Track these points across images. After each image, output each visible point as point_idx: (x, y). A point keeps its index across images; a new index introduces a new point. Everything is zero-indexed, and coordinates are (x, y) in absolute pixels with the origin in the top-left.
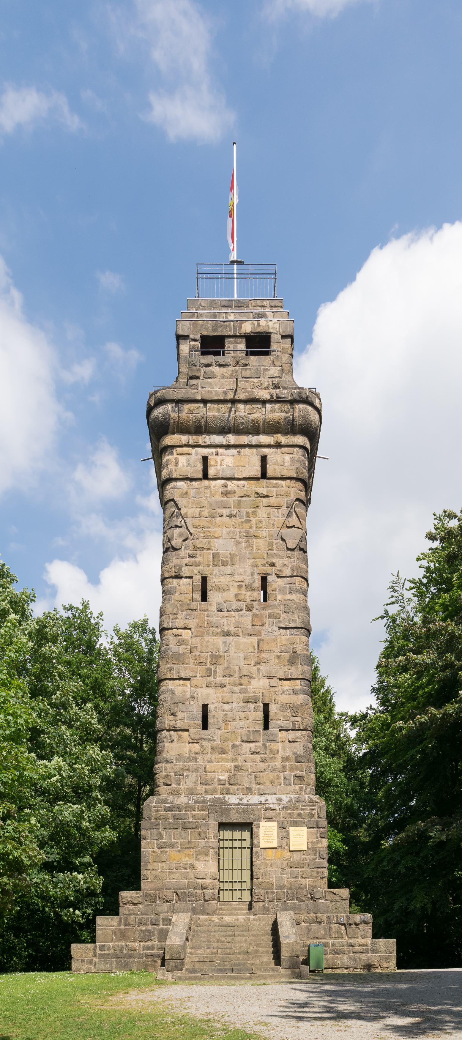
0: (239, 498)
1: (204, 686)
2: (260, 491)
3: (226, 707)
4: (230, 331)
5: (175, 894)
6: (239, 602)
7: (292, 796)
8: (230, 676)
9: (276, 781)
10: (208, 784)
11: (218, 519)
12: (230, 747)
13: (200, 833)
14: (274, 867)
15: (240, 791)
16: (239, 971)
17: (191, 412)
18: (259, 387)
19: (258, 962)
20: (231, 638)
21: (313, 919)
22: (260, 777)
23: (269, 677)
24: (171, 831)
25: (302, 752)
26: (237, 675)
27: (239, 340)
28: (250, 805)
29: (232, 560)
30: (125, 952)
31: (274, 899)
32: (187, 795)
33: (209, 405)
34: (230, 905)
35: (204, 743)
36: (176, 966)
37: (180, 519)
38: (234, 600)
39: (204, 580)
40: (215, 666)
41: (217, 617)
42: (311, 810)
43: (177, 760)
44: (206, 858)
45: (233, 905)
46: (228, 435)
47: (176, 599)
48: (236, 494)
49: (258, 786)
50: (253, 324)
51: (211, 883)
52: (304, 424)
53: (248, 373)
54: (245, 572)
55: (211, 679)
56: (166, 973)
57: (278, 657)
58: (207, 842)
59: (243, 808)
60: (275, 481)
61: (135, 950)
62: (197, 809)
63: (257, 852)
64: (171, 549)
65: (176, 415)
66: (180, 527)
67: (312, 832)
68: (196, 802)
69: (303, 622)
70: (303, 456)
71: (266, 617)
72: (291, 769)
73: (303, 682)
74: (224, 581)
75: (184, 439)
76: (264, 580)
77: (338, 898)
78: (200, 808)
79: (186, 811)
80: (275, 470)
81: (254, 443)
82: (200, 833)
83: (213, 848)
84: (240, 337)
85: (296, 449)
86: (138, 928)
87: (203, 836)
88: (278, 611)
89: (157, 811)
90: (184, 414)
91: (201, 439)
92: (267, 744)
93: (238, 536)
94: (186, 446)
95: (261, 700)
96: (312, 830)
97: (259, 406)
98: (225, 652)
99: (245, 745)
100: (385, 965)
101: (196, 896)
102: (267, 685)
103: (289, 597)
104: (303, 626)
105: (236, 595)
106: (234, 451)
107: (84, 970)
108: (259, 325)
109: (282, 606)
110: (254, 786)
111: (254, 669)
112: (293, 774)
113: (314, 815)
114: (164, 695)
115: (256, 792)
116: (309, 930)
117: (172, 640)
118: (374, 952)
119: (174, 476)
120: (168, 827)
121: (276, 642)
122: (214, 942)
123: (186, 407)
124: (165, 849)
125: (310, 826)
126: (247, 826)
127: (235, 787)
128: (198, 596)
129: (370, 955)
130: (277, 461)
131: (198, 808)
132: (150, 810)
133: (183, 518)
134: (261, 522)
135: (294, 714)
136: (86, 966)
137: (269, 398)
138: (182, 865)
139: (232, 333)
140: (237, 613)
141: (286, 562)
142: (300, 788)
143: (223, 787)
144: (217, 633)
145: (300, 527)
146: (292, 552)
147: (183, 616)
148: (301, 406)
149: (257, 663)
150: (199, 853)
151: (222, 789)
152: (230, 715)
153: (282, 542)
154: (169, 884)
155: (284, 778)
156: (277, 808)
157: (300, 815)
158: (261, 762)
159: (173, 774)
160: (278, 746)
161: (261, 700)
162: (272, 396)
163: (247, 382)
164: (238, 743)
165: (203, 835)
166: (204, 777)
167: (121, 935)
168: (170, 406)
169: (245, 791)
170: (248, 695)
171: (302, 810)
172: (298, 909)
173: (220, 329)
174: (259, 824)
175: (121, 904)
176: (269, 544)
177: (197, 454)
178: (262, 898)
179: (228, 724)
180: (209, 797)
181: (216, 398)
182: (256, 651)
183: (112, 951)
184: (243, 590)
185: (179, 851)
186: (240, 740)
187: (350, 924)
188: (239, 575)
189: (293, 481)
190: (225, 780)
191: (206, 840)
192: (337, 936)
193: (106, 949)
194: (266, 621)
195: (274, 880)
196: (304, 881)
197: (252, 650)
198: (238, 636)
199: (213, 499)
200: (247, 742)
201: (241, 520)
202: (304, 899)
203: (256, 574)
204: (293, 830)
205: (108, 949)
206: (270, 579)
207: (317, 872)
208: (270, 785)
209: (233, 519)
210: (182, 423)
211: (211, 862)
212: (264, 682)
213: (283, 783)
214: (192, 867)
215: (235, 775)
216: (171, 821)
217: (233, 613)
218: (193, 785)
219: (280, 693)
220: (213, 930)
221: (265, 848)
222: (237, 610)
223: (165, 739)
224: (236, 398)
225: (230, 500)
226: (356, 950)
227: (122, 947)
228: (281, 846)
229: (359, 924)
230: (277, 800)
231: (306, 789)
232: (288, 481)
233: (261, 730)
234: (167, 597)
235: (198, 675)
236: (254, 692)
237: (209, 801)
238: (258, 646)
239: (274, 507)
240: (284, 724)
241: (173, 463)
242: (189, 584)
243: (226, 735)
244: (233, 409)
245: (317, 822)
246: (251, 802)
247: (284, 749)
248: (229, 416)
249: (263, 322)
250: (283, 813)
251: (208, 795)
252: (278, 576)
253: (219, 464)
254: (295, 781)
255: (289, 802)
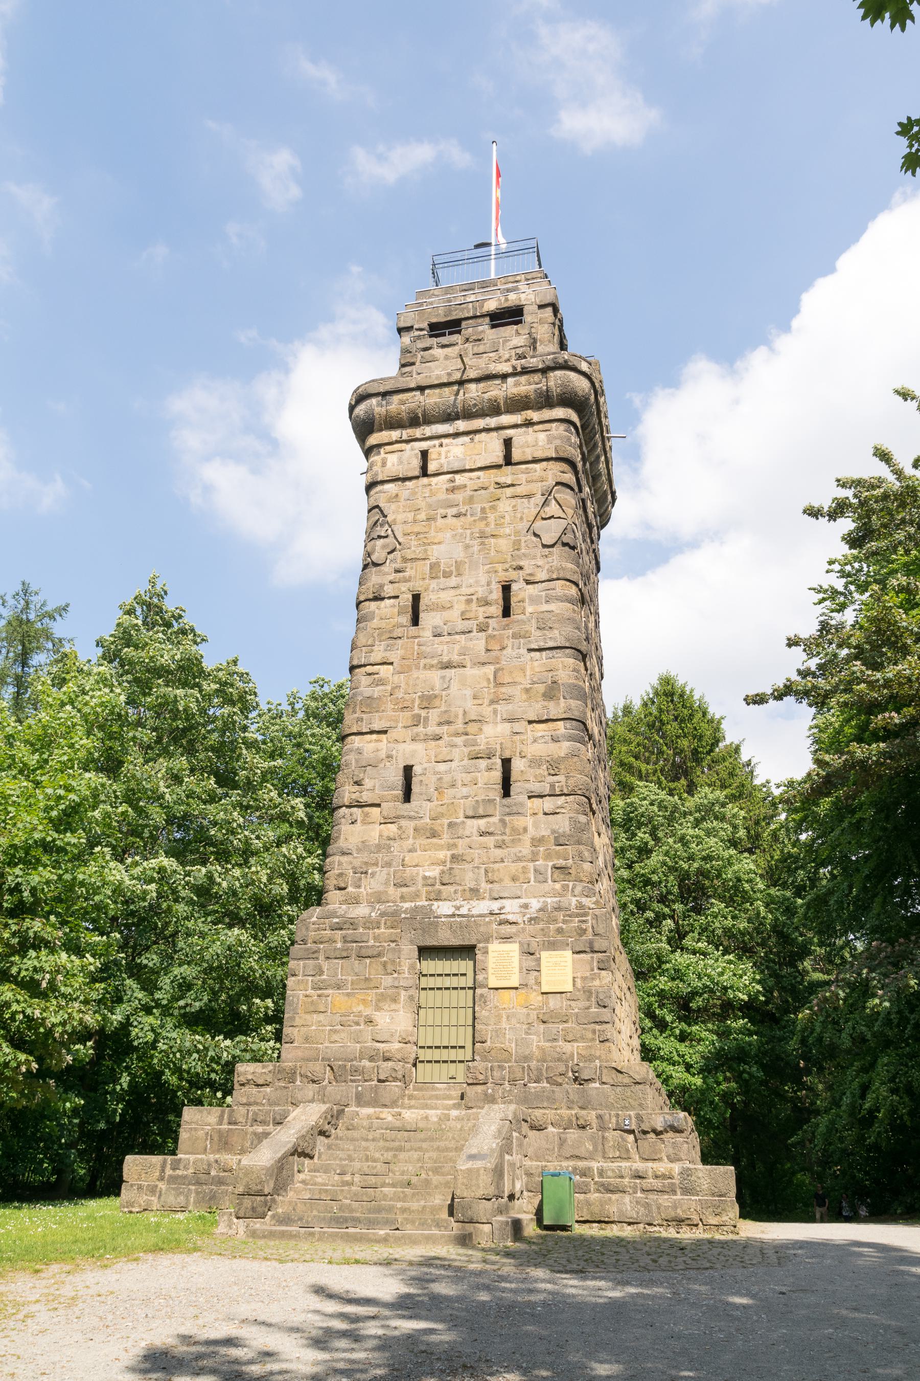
0: (472, 493)
1: (408, 740)
2: (502, 480)
3: (442, 767)
4: (468, 312)
5: (328, 1068)
6: (467, 622)
7: (549, 900)
8: (449, 723)
9: (522, 876)
10: (406, 885)
11: (440, 521)
12: (446, 827)
13: (384, 965)
14: (514, 1021)
15: (459, 894)
16: (371, 1223)
17: (403, 403)
18: (498, 360)
19: (415, 1205)
20: (453, 670)
21: (570, 1121)
22: (493, 871)
23: (511, 720)
24: (337, 961)
25: (567, 829)
26: (460, 720)
27: (480, 320)
28: (473, 916)
29: (457, 569)
30: (213, 1173)
31: (504, 1079)
32: (371, 904)
33: (427, 391)
34: (433, 1089)
35: (403, 823)
36: (253, 1209)
37: (386, 527)
38: (460, 618)
39: (416, 598)
40: (426, 710)
41: (433, 645)
42: (580, 921)
43: (359, 850)
44: (393, 1006)
45: (437, 1089)
46: (457, 422)
47: (374, 626)
48: (468, 489)
49: (491, 886)
50: (500, 300)
51: (399, 1050)
52: (564, 393)
53: (481, 349)
54: (477, 582)
55: (420, 729)
56: (235, 1220)
57: (527, 691)
58: (396, 978)
59: (461, 923)
60: (524, 466)
61: (230, 1171)
62: (382, 925)
63: (482, 995)
64: (371, 565)
65: (384, 409)
66: (386, 537)
67: (582, 960)
68: (383, 914)
69: (568, 640)
70: (566, 431)
71: (508, 637)
72: (548, 857)
73: (569, 724)
74: (445, 596)
75: (395, 434)
76: (506, 589)
77: (627, 1080)
78: (389, 923)
79: (365, 928)
80: (524, 452)
81: (493, 426)
82: (384, 965)
83: (406, 989)
84: (483, 316)
85: (554, 425)
86: (251, 1129)
87: (390, 969)
88: (527, 627)
89: (318, 929)
90: (394, 406)
91: (418, 432)
92: (507, 818)
93: (468, 538)
94: (397, 442)
95: (498, 754)
96: (582, 955)
97: (498, 382)
98: (443, 690)
99: (469, 822)
100: (714, 1221)
101: (363, 1073)
102: (508, 732)
103: (545, 607)
104: (567, 645)
105: (463, 613)
106: (466, 439)
107: (140, 1206)
108: (507, 300)
109: (534, 621)
110: (484, 886)
111: (487, 711)
112: (550, 864)
113: (586, 930)
114: (347, 757)
115: (487, 895)
116: (562, 1142)
117: (365, 681)
118: (686, 1191)
119: (380, 478)
120: (332, 955)
121: (523, 670)
122: (360, 1160)
123: (396, 398)
124: (326, 992)
125: (578, 950)
126: (467, 951)
127: (451, 889)
128: (406, 619)
129: (679, 1197)
130: (526, 442)
131: (385, 924)
132: (307, 929)
133: (390, 526)
134: (503, 517)
135: (552, 772)
136: (145, 1197)
137: (510, 370)
138: (351, 1018)
139: (471, 314)
140: (463, 636)
141: (540, 563)
142: (563, 886)
143: (430, 888)
144: (432, 666)
145: (563, 515)
146: (551, 549)
147: (382, 648)
148: (558, 373)
149: (492, 702)
150: (382, 998)
151: (428, 893)
152: (447, 779)
153: (534, 539)
154: (329, 1051)
155: (535, 870)
156: (520, 921)
157: (560, 931)
158: (495, 847)
159: (351, 871)
160: (529, 821)
161: (498, 754)
162: (514, 368)
163: (480, 358)
164: (458, 821)
165: (390, 968)
166: (400, 874)
167: (220, 1140)
168: (374, 401)
169: (468, 894)
170: (477, 748)
171: (564, 922)
172: (548, 1098)
173: (454, 313)
174: (487, 948)
175: (236, 1086)
176: (514, 543)
177: (412, 450)
178: (481, 1077)
179: (443, 792)
180: (407, 905)
181: (436, 382)
182: (492, 685)
183: (191, 1171)
184: (474, 606)
185: (348, 995)
186: (461, 815)
187: (645, 1132)
188: (467, 587)
189: (551, 463)
190: (435, 878)
191: (396, 975)
192: (617, 1154)
193: (181, 1167)
194: (509, 643)
195: (513, 1045)
196: (568, 1048)
197: (485, 684)
198: (464, 667)
199: (434, 498)
200: (473, 817)
201: (473, 518)
202: (559, 1080)
203: (494, 583)
204: (546, 956)
205: (186, 1168)
206: (514, 587)
207: (594, 1032)
208: (512, 884)
209: (462, 518)
210: (391, 417)
211: (401, 1012)
212: (505, 728)
213: (532, 879)
214: (370, 1021)
215: (451, 869)
216: (339, 945)
217: (457, 637)
218: (382, 888)
219: (529, 742)
220: (370, 1137)
221: (497, 989)
222: (463, 633)
223: (343, 820)
224: (465, 377)
225: (459, 497)
226: (649, 1187)
227: (209, 1165)
228: (526, 985)
229: (661, 1133)
230: (521, 907)
231: (573, 888)
232: (545, 463)
233: (498, 799)
234: (361, 625)
235: (400, 725)
236: (487, 743)
237: (405, 912)
238: (495, 677)
239: (522, 497)
240: (536, 787)
241: (379, 464)
242: (394, 606)
243: (440, 809)
244: (461, 392)
245: (591, 943)
246: (475, 912)
247: (536, 825)
248: (456, 399)
249: (512, 296)
250: (530, 928)
251: (406, 902)
252: (528, 582)
253: (443, 456)
254: (555, 876)
255: (541, 910)
